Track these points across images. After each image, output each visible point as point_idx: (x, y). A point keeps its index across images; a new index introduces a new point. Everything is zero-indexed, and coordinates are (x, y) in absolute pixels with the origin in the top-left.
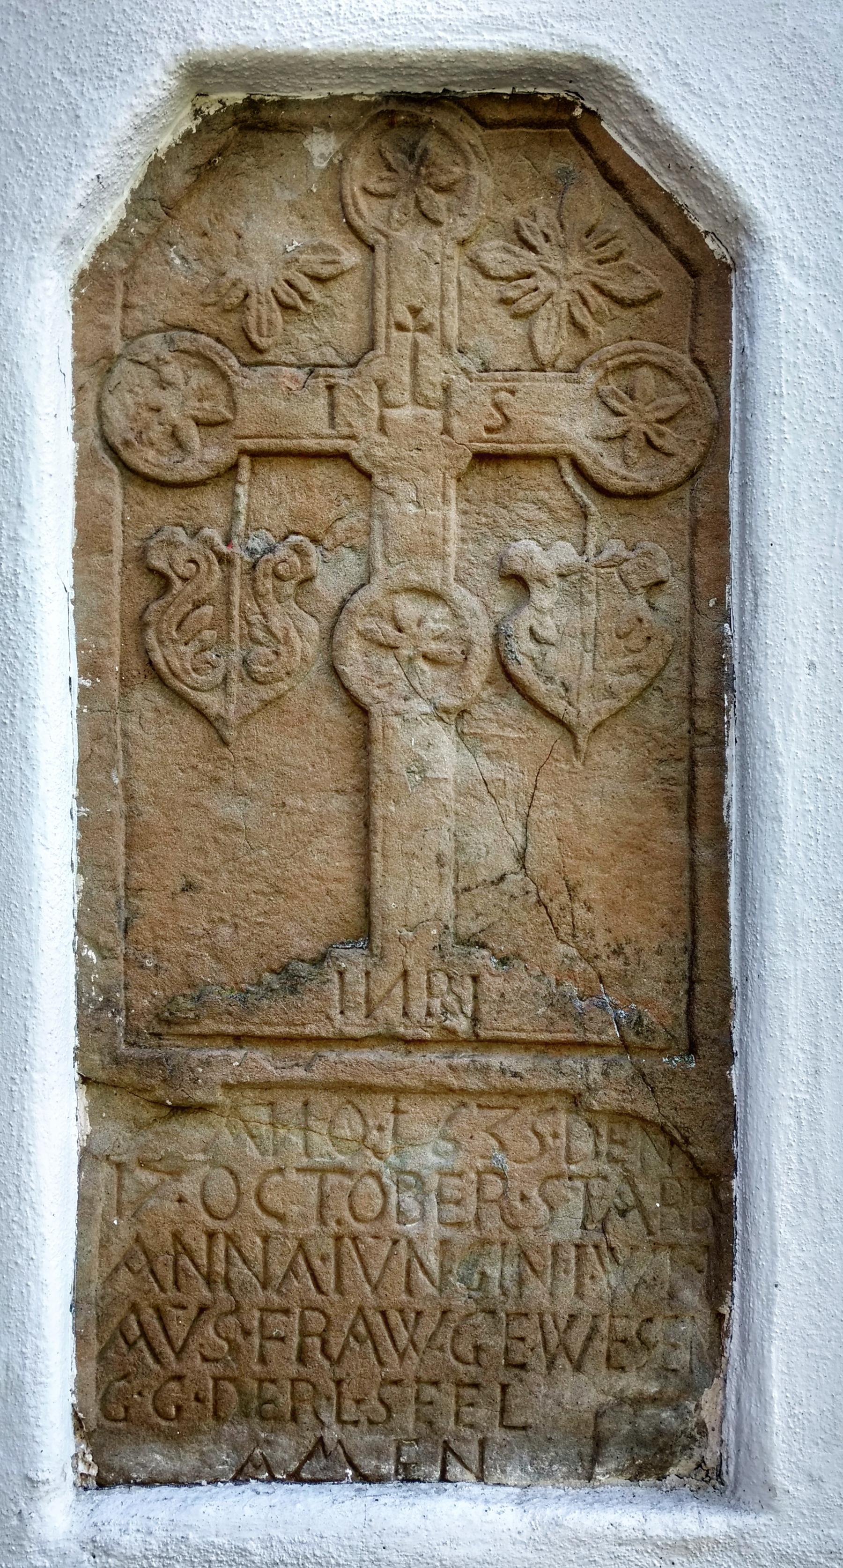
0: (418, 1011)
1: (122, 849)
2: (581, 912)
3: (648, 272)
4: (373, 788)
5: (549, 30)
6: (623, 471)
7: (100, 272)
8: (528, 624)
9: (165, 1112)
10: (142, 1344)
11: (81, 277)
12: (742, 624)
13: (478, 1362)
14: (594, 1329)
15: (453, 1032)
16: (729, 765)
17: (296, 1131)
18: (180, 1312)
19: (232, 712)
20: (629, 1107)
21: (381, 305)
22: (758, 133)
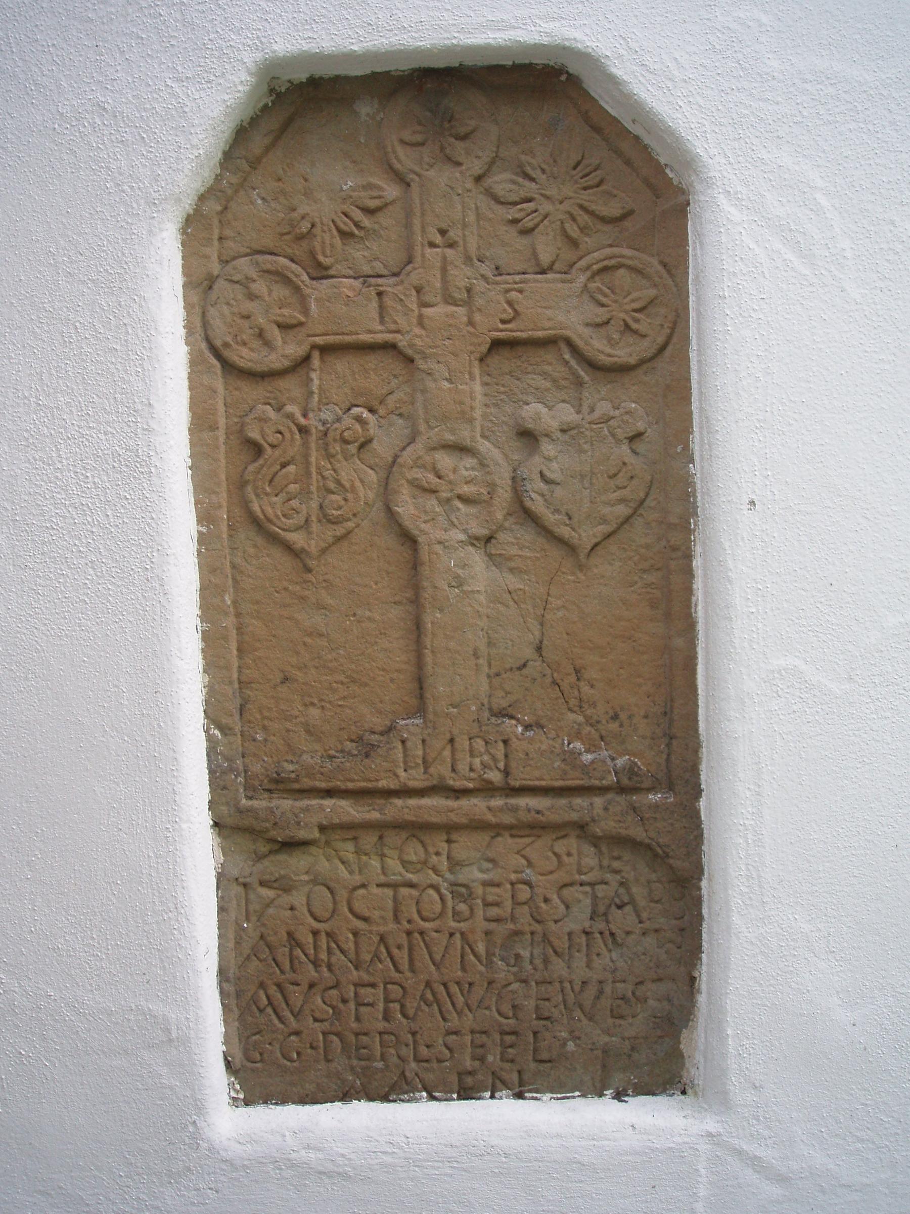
0: (463, 767)
1: (235, 652)
2: (585, 688)
3: (624, 195)
4: (422, 600)
5: (538, 29)
6: (608, 350)
7: (202, 215)
8: (539, 470)
9: (276, 847)
10: (269, 1010)
11: (187, 220)
12: (702, 467)
13: (515, 1016)
14: (601, 992)
15: (489, 782)
16: (695, 573)
17: (375, 857)
18: (296, 988)
19: (313, 547)
20: (623, 832)
21: (417, 228)
22: (699, 99)
